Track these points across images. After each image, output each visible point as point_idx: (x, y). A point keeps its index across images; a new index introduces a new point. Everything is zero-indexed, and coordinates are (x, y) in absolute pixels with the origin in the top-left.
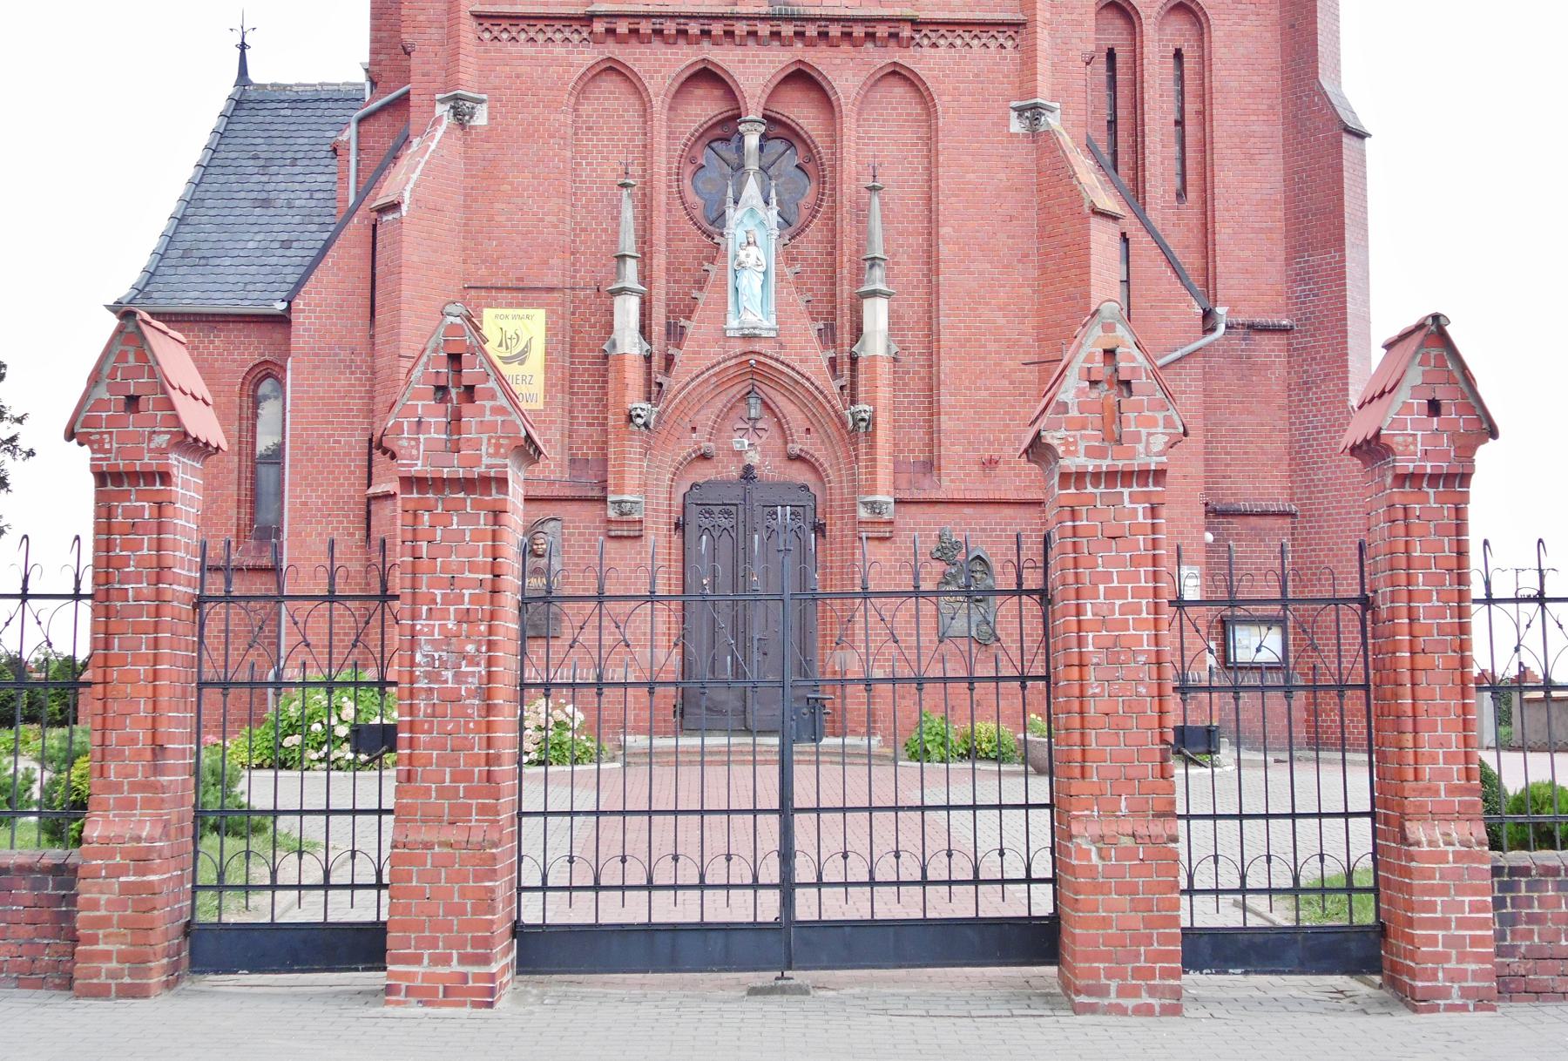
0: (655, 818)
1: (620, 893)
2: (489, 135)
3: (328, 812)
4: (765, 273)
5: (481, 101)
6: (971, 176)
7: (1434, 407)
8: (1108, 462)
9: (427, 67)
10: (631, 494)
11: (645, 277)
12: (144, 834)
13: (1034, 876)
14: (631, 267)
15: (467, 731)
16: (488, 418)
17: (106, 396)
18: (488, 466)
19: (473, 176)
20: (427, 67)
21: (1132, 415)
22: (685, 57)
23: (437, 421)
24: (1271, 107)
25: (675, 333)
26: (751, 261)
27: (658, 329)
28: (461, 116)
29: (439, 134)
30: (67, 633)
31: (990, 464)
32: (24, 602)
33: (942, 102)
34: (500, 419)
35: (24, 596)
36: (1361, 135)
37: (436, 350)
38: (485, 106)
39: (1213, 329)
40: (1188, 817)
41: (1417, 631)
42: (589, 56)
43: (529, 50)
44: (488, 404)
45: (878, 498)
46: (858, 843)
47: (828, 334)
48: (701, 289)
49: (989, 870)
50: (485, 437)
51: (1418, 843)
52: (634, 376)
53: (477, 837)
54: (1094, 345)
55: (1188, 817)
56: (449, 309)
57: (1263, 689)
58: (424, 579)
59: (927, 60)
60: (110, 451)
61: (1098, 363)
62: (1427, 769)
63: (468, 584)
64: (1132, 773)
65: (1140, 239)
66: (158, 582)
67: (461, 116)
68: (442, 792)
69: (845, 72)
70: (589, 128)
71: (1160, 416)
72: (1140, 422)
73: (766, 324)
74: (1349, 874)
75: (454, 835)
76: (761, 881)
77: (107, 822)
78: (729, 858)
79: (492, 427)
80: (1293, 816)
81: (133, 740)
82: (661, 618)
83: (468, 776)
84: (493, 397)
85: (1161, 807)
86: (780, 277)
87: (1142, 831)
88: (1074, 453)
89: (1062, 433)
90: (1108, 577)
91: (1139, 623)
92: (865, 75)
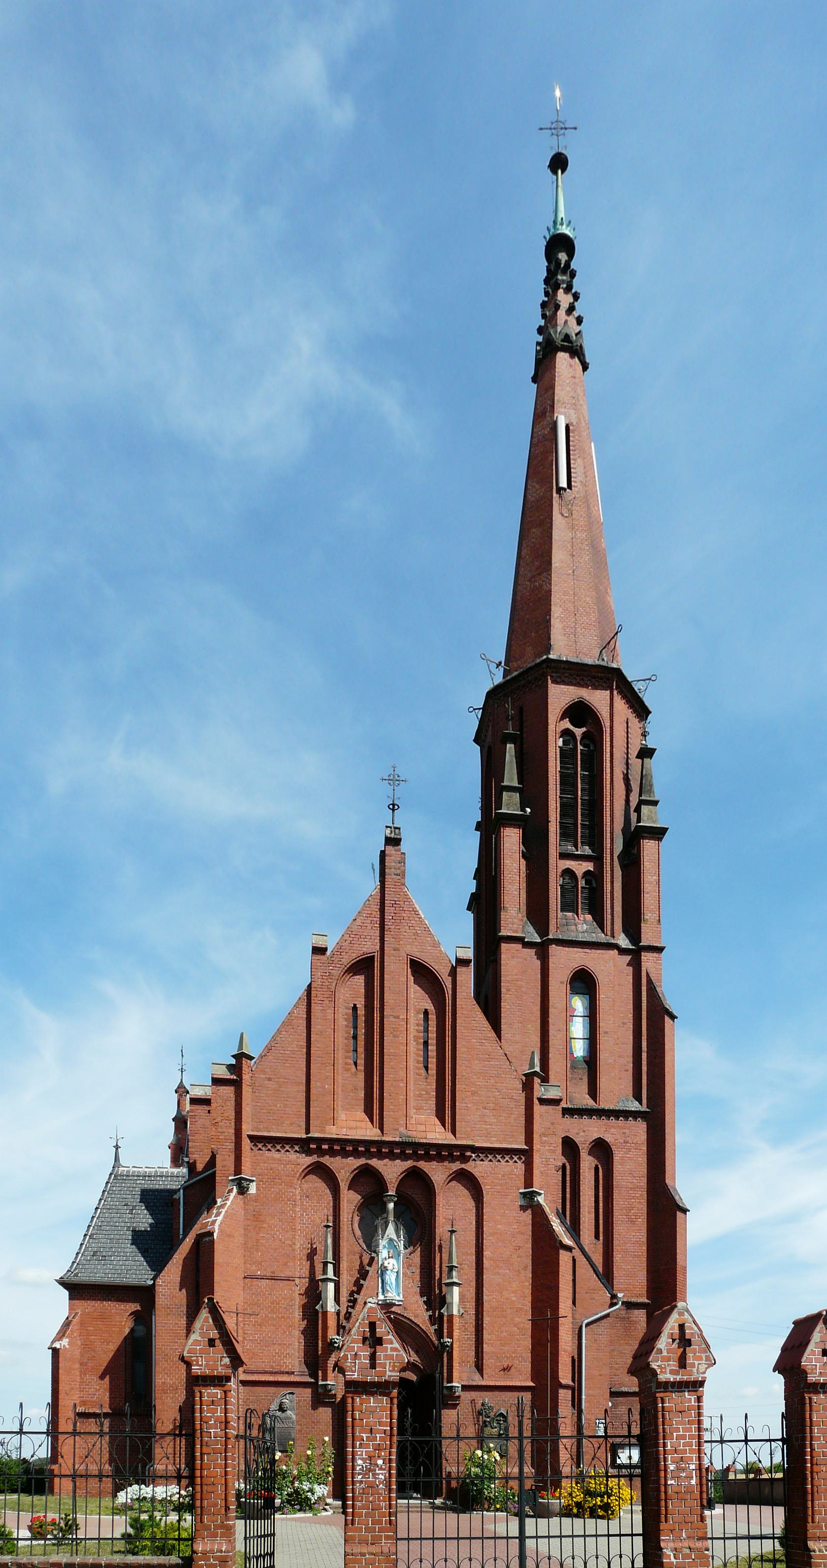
3: (408, 1539)
4: (397, 1272)
5: (253, 1181)
8: (680, 1377)
9: (225, 1163)
10: (331, 1380)
11: (337, 1272)
12: (223, 1549)
14: (330, 1267)
15: (379, 1501)
16: (389, 1353)
17: (199, 1339)
19: (248, 1219)
20: (225, 1163)
21: (691, 1355)
22: (354, 1163)
25: (353, 1302)
26: (390, 1267)
28: (242, 1191)
30: (35, 1449)
31: (507, 1369)
33: (486, 1189)
34: (395, 1353)
35: (21, 1432)
37: (363, 1320)
38: (254, 1183)
39: (616, 1304)
40: (712, 1539)
42: (307, 1160)
44: (389, 1346)
45: (454, 1384)
47: (429, 1305)
48: (365, 1280)
50: (388, 1362)
51: (814, 1551)
52: (332, 1323)
54: (675, 1322)
56: (369, 1300)
58: (357, 1429)
59: (478, 1168)
60: (201, 1365)
61: (676, 1331)
62: (817, 1517)
63: (379, 1432)
64: (687, 1520)
65: (581, 1260)
67: (242, 1191)
68: (368, 1530)
69: (438, 1172)
70: (307, 1197)
71: (704, 1356)
72: (695, 1358)
73: (398, 1298)
77: (205, 1544)
78: (470, 1560)
79: (391, 1357)
80: (573, 1536)
81: (216, 1505)
83: (380, 1522)
84: (392, 1343)
85: (700, 1535)
87: (692, 1546)
88: (665, 1373)
89: (659, 1363)
90: (678, 1430)
91: (691, 1451)
92: (448, 1174)
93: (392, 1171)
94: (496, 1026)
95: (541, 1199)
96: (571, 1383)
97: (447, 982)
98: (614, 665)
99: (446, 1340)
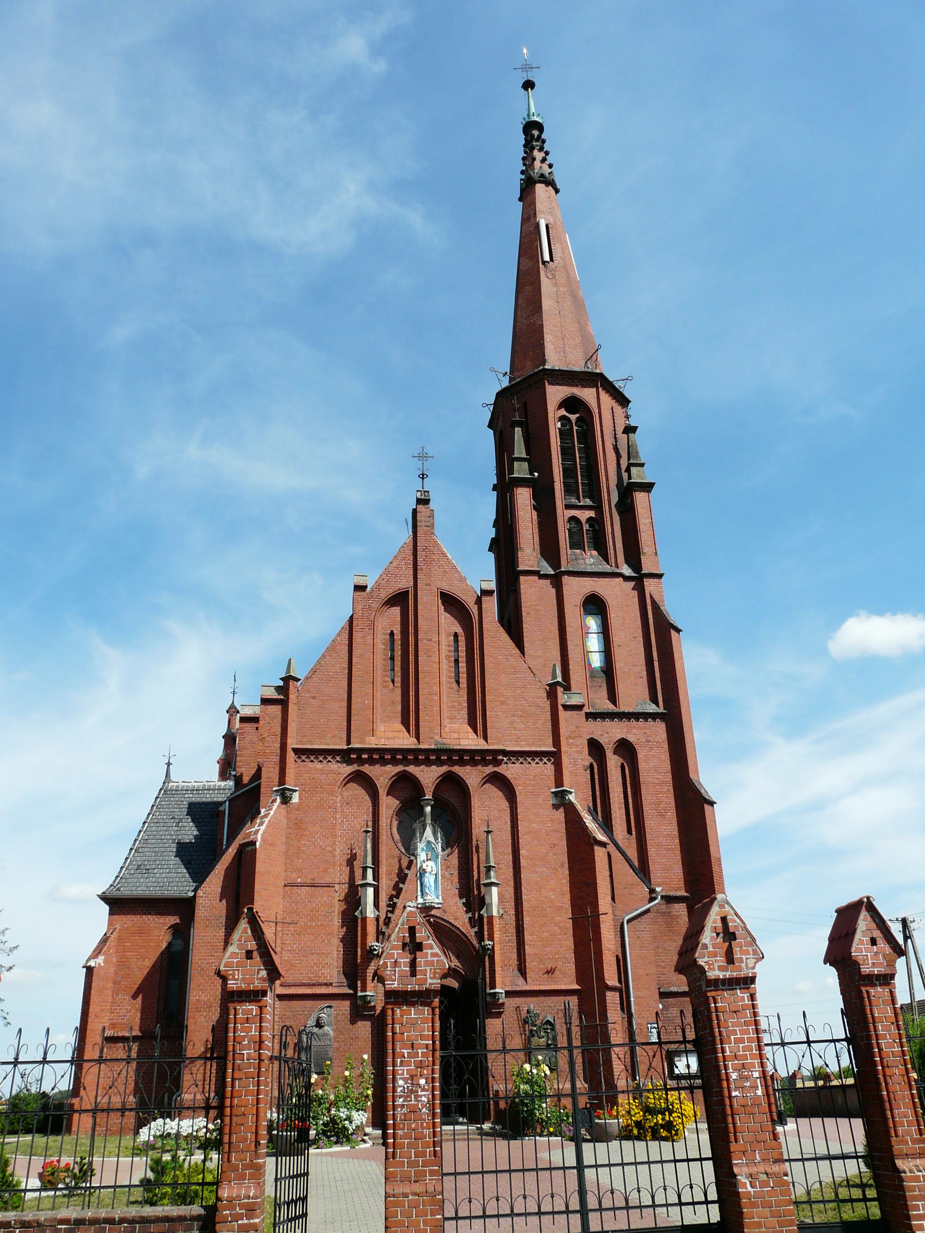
0: (513, 1174)
1: (524, 1218)
2: (299, 807)
4: (436, 875)
5: (296, 791)
6: (534, 825)
7: (873, 942)
10: (370, 991)
11: (376, 877)
12: (251, 1194)
13: (657, 1203)
16: (429, 959)
17: (237, 951)
18: (431, 984)
21: (738, 949)
22: (393, 770)
23: (405, 960)
24: (668, 790)
25: (392, 907)
26: (428, 870)
27: (383, 903)
28: (285, 800)
29: (275, 807)
31: (550, 972)
32: (15, 1066)
33: (518, 789)
34: (435, 959)
35: (16, 1063)
36: (712, 803)
37: (403, 925)
39: (655, 899)
41: (883, 1056)
42: (348, 769)
43: (319, 766)
44: (430, 951)
45: (497, 990)
46: (531, 1190)
47: (469, 907)
48: (404, 883)
49: (634, 1199)
50: (428, 968)
52: (371, 929)
53: (430, 1189)
54: (716, 915)
55: (790, 1160)
56: (408, 904)
57: (231, 1107)
58: (398, 1044)
59: (510, 770)
60: (237, 980)
61: (719, 924)
62: (900, 1129)
66: (260, 1049)
67: (285, 800)
69: (472, 776)
71: (750, 949)
73: (437, 901)
74: (808, 1193)
75: (417, 1188)
76: (515, 1212)
77: (231, 1188)
82: (214, 1065)
83: (423, 1154)
84: (432, 948)
86: (443, 876)
87: (769, 1171)
88: (713, 969)
89: (706, 959)
92: (481, 777)
93: (428, 776)
94: (523, 652)
95: (572, 797)
96: (618, 985)
97: (474, 610)
98: (598, 371)
99: (487, 942)
